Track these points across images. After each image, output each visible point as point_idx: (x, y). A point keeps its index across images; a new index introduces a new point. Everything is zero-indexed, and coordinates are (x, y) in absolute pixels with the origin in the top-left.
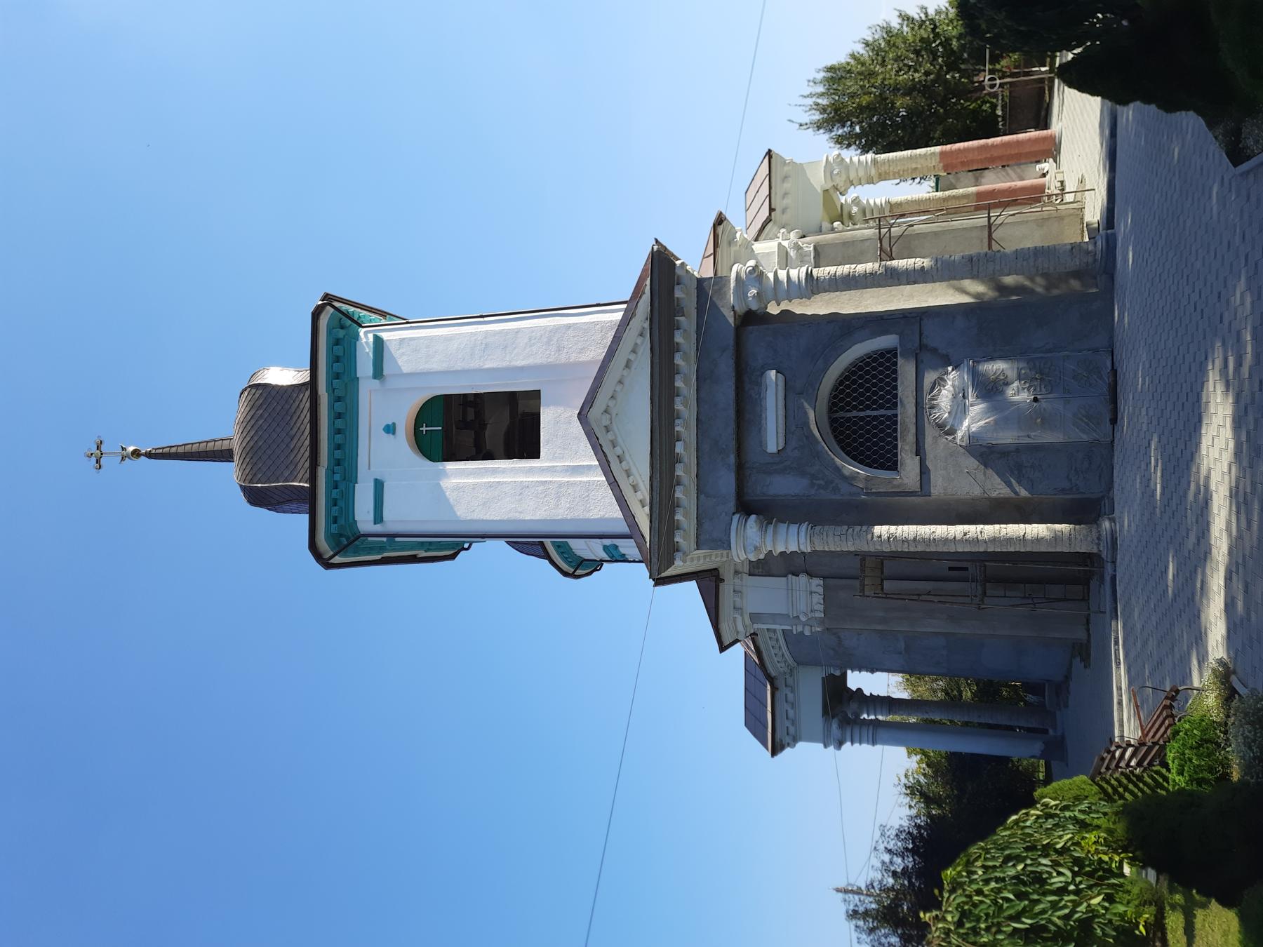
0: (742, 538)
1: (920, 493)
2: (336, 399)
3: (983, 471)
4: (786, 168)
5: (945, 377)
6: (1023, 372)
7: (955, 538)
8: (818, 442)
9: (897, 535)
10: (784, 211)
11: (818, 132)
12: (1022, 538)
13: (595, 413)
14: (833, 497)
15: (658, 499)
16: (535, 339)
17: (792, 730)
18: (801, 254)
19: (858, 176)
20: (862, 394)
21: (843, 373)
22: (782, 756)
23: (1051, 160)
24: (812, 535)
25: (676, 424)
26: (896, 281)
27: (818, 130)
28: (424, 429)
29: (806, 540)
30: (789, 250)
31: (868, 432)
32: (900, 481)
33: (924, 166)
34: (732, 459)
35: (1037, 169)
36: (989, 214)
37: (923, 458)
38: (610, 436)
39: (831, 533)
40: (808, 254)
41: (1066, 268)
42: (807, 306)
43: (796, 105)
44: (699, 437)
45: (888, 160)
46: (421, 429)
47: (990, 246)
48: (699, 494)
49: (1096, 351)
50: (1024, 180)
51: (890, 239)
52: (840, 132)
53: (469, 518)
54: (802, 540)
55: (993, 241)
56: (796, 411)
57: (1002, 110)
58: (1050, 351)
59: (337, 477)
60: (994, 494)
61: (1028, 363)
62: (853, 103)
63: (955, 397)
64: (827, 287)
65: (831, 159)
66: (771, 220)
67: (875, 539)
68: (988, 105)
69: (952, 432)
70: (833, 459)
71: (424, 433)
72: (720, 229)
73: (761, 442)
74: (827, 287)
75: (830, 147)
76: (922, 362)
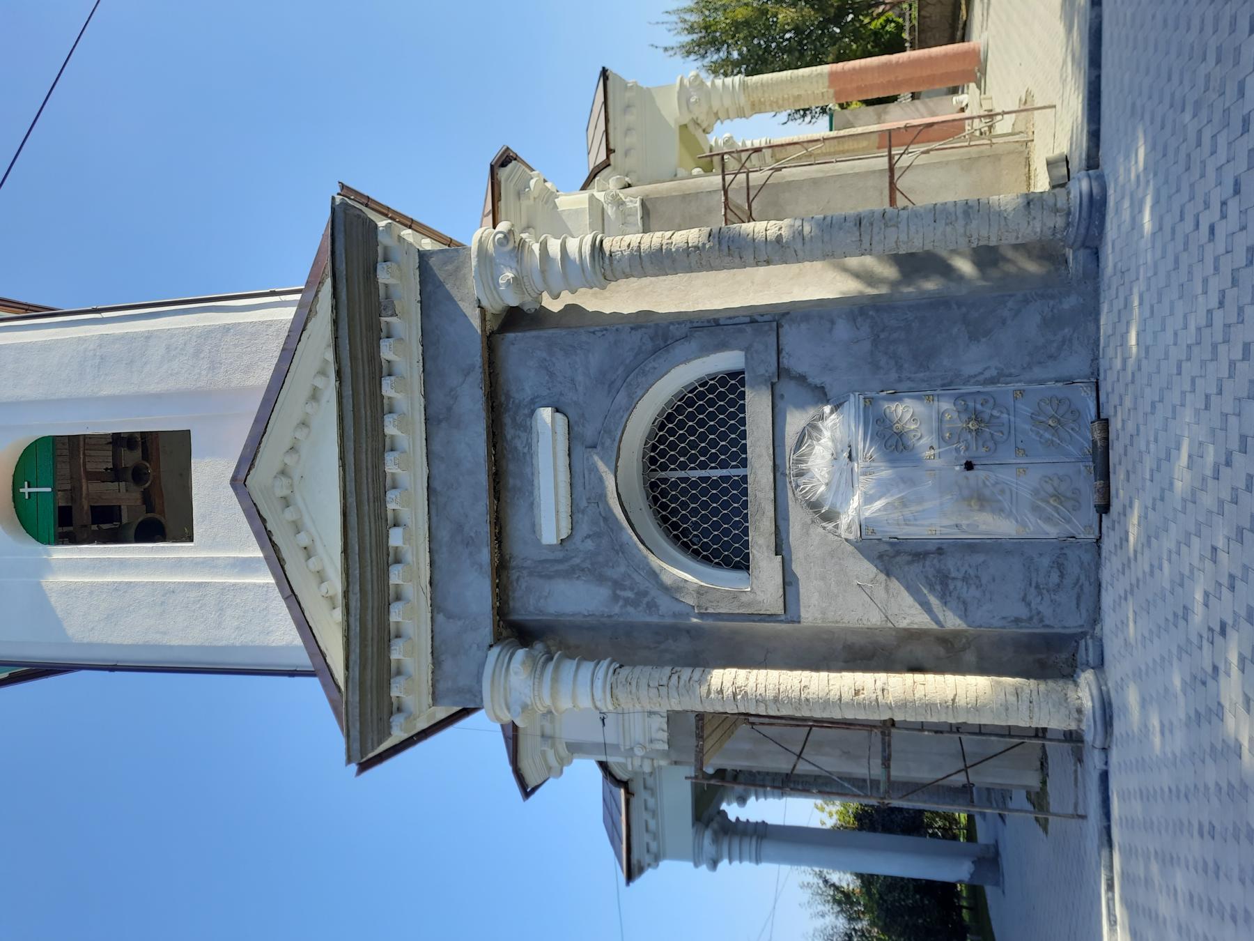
0: (502, 689)
1: (783, 618)
3: (883, 585)
4: (628, 94)
5: (820, 424)
6: (947, 417)
7: (840, 699)
8: (621, 528)
9: (748, 689)
10: (627, 153)
11: (687, 59)
12: (950, 703)
13: (260, 478)
14: (649, 619)
15: (358, 629)
16: (176, 348)
17: (653, 846)
18: (623, 213)
19: (723, 105)
20: (693, 445)
21: (663, 410)
22: (639, 882)
23: (972, 85)
24: (614, 686)
25: (388, 499)
26: (737, 260)
27: (688, 56)
28: (26, 490)
29: (604, 692)
30: (605, 205)
31: (705, 505)
32: (752, 596)
33: (809, 92)
34: (485, 555)
35: (954, 102)
36: (890, 151)
37: (787, 557)
38: (289, 515)
39: (643, 682)
40: (632, 213)
41: (1017, 238)
42: (606, 298)
43: (658, 23)
44: (434, 519)
45: (762, 84)
46: (21, 490)
47: (892, 201)
48: (435, 614)
49: (1070, 381)
50: (937, 115)
51: (748, 189)
52: (715, 57)
53: (85, 641)
54: (598, 693)
55: (897, 192)
56: (586, 476)
57: (910, 34)
58: (992, 381)
60: (904, 624)
61: (955, 404)
62: (726, 19)
63: (835, 457)
64: (628, 270)
65: (686, 82)
66: (609, 165)
67: (712, 696)
68: (893, 25)
69: (830, 517)
70: (646, 557)
71: (27, 497)
72: (503, 173)
73: (533, 525)
74: (628, 270)
75: (671, 56)
76: (782, 396)
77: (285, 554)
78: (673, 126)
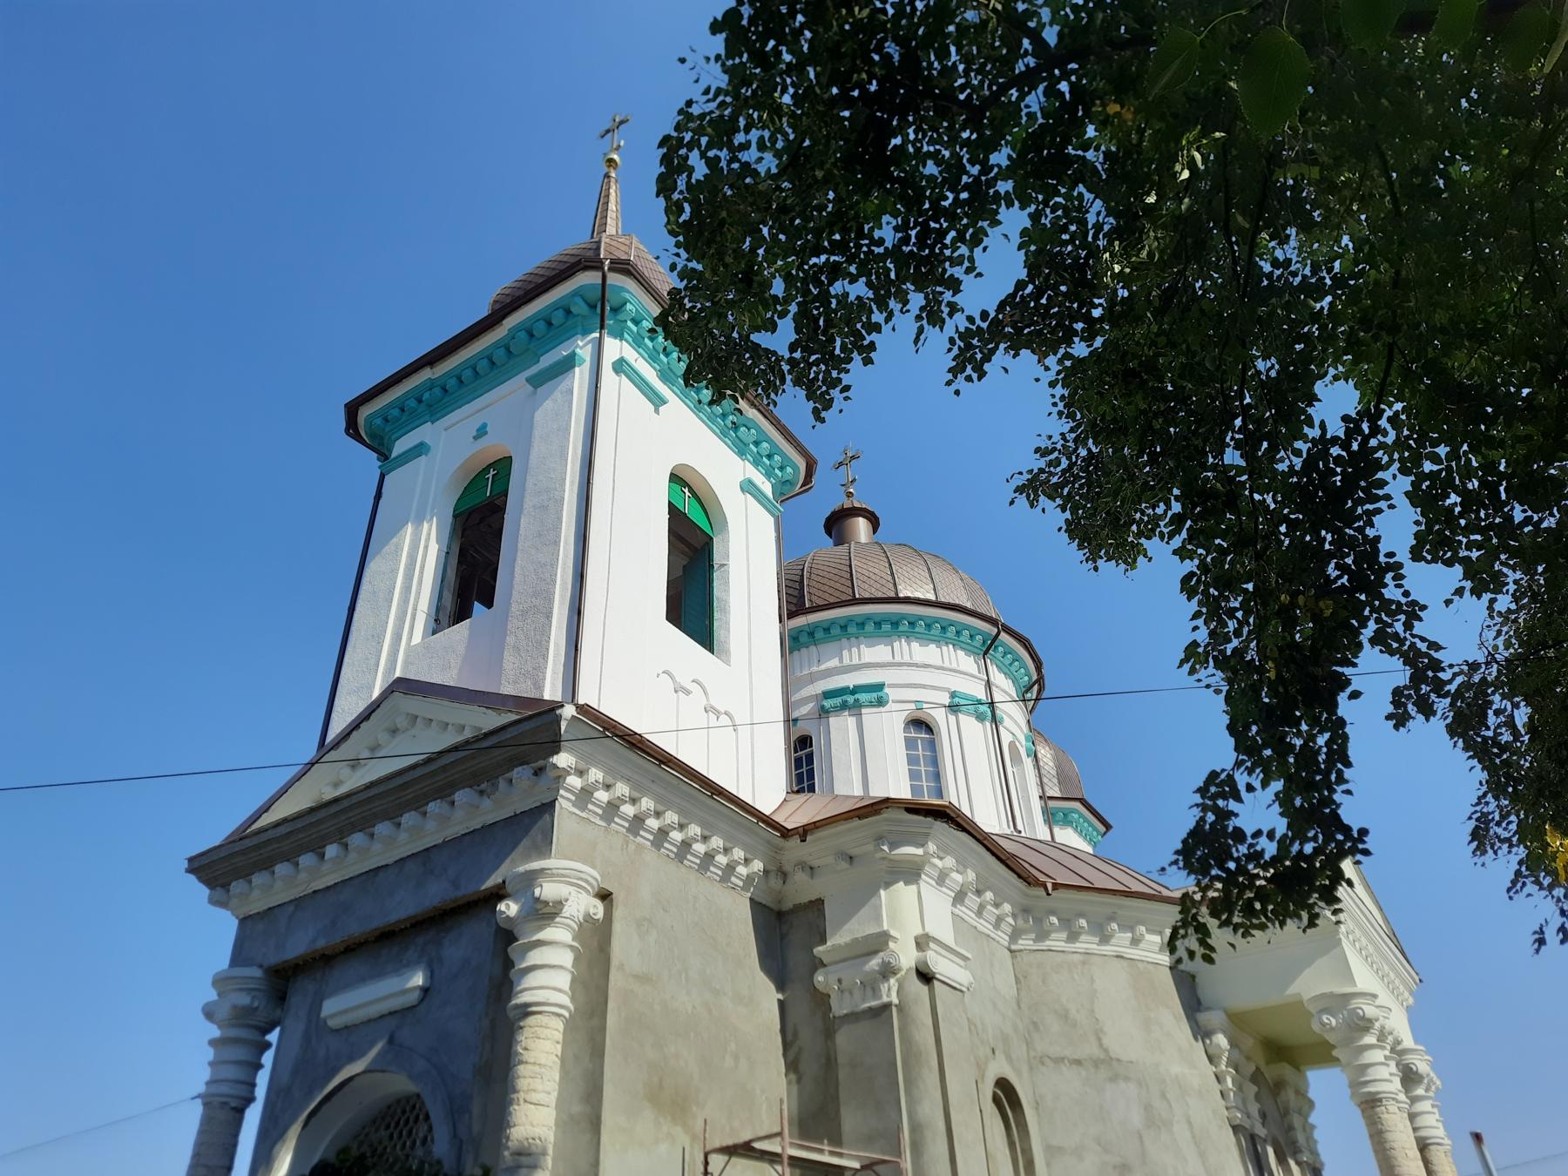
2: (506, 346)
40: (876, 992)
59: (426, 396)
78: (1288, 992)
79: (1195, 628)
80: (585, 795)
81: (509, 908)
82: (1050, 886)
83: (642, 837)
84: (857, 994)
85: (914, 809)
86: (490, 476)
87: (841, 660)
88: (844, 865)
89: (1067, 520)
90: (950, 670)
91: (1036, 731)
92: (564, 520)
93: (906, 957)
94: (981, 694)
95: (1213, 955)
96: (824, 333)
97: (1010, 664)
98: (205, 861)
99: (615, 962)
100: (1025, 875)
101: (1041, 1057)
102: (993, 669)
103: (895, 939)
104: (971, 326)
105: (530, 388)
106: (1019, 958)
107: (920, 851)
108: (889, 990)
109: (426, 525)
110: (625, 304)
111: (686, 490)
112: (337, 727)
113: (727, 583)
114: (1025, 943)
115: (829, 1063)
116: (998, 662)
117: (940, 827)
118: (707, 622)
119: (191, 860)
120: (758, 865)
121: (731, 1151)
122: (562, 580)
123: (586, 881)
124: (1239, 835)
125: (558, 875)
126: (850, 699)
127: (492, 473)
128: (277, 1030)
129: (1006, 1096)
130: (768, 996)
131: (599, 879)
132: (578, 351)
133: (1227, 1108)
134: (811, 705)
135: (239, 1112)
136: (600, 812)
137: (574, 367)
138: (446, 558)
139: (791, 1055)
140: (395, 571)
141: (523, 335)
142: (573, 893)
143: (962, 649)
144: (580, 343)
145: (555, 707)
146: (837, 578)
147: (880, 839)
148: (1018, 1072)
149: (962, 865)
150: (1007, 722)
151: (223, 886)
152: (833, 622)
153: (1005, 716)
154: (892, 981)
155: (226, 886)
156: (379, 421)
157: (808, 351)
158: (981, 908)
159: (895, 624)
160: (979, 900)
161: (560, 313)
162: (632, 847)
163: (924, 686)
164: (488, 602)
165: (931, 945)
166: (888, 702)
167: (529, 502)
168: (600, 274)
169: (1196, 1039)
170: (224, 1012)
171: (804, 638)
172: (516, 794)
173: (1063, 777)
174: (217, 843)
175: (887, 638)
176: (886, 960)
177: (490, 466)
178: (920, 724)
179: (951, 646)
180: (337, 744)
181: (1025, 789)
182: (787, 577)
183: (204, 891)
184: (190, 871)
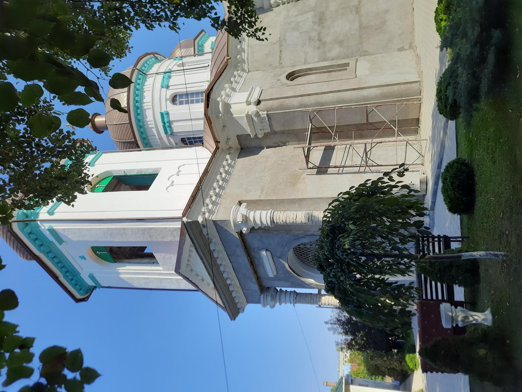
2: (47, 253)
38: (200, 278)
40: (263, 118)
59: (70, 278)
77: (197, 284)
79: (164, 26)
80: (211, 212)
81: (245, 230)
82: (228, 58)
83: (221, 193)
84: (264, 125)
85: (207, 106)
86: (99, 253)
87: (153, 128)
88: (226, 129)
89: (117, 58)
90: (153, 88)
91: (170, 56)
92: (115, 227)
93: (253, 108)
94: (160, 77)
95: (263, 28)
96: (63, 148)
97: (149, 65)
98: (232, 316)
99: (258, 198)
100: (225, 67)
101: (280, 64)
102: (151, 72)
103: (248, 112)
104: (57, 97)
105: (63, 244)
106: (251, 69)
107: (221, 103)
108: (263, 114)
109: (120, 271)
110: (24, 213)
111: (97, 186)
112: (191, 287)
113: (131, 170)
114: (246, 67)
115: (283, 133)
116: (148, 69)
117: (212, 96)
118: (146, 176)
119: (231, 320)
120: (228, 157)
121: (307, 162)
122: (138, 226)
123: (236, 209)
124: (230, 18)
125: (235, 217)
126: (167, 124)
127: (98, 252)
128: (277, 288)
129: (291, 76)
130: (266, 152)
131: (235, 205)
132: (47, 228)
133: (292, 2)
134: (170, 138)
135: (297, 294)
136: (215, 207)
137: (53, 229)
138: (131, 263)
139: (281, 144)
140: (137, 278)
141: (42, 248)
142: (240, 212)
143: (144, 83)
144: (43, 228)
145: (183, 224)
146: (122, 130)
147: (218, 117)
148: (285, 72)
149: (223, 88)
150: (170, 67)
151: (239, 310)
152: (139, 131)
153: (168, 68)
154: (260, 113)
155: (239, 309)
156: (82, 292)
157: (72, 154)
158: (236, 82)
159: (138, 108)
160: (234, 83)
161: (31, 236)
162: (225, 196)
163: (160, 98)
164: (144, 248)
165: (249, 100)
166: (167, 111)
167: (109, 239)
168: (13, 223)
169: (273, 10)
170: (272, 303)
171: (146, 141)
172: (213, 232)
173: (187, 47)
174: (227, 314)
175: (143, 111)
176: (254, 115)
177: (96, 254)
178: (174, 99)
179: (144, 87)
180: (197, 286)
181: (194, 62)
182: (123, 148)
183: (240, 315)
184: (235, 319)
